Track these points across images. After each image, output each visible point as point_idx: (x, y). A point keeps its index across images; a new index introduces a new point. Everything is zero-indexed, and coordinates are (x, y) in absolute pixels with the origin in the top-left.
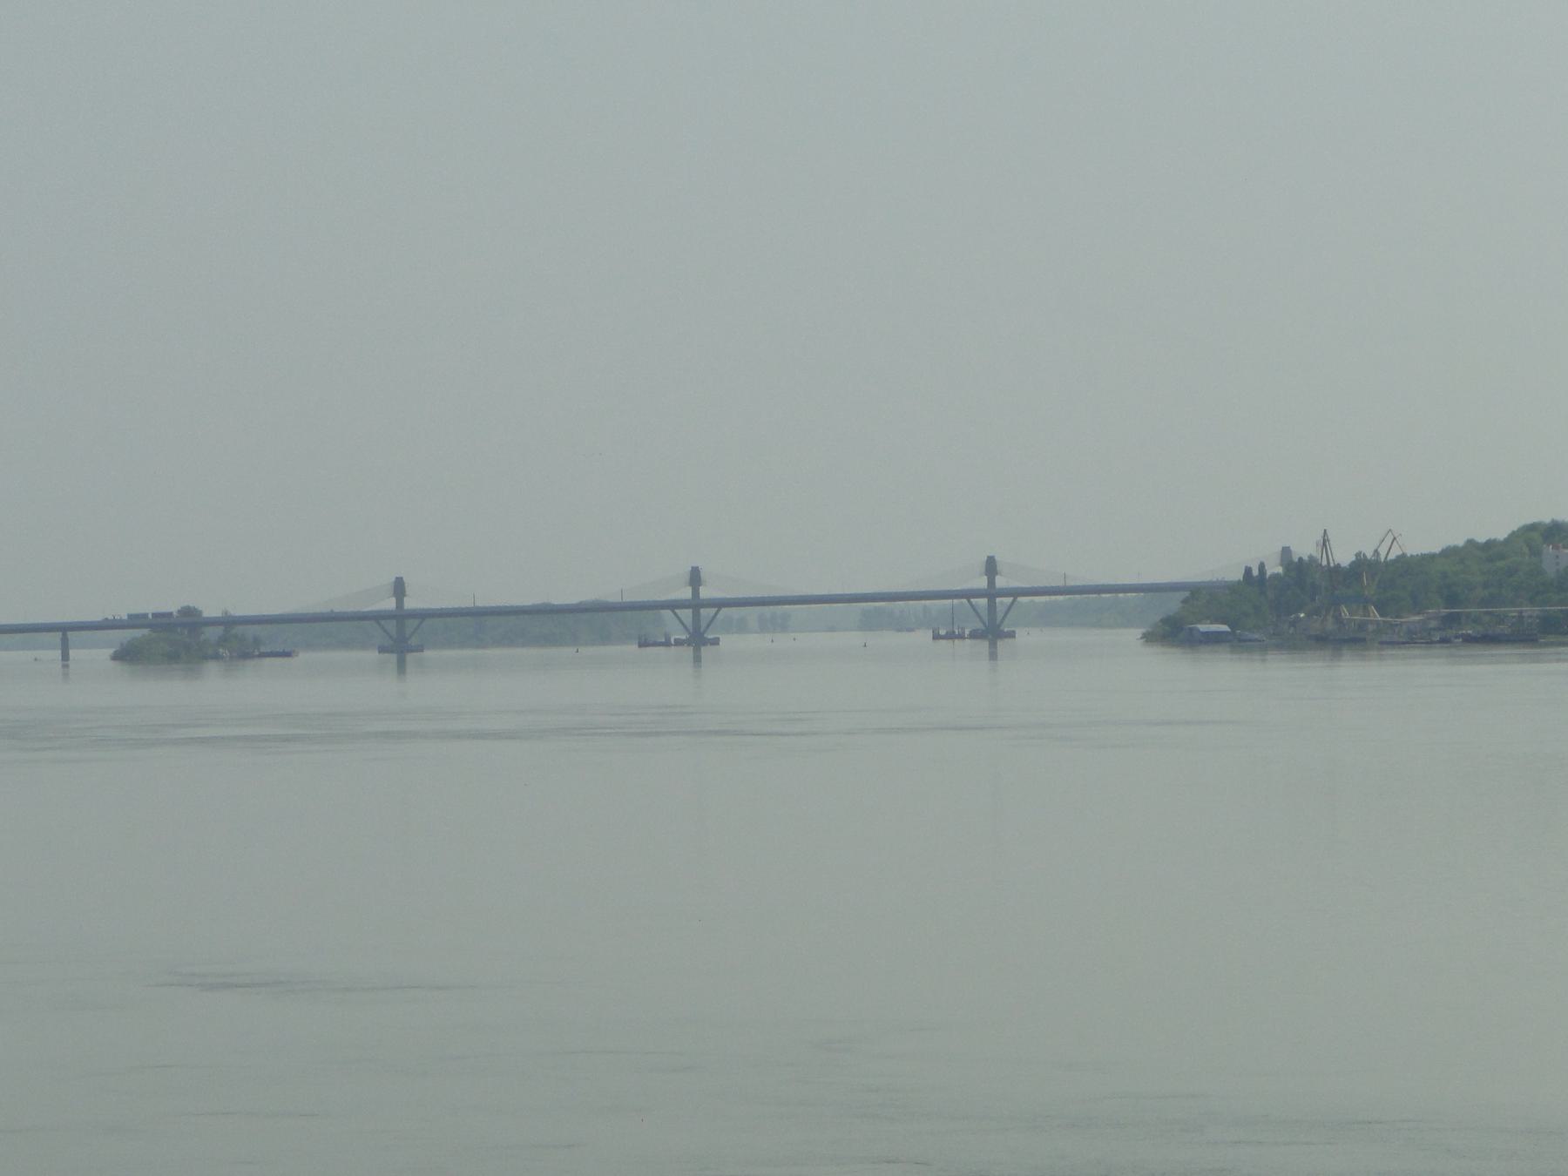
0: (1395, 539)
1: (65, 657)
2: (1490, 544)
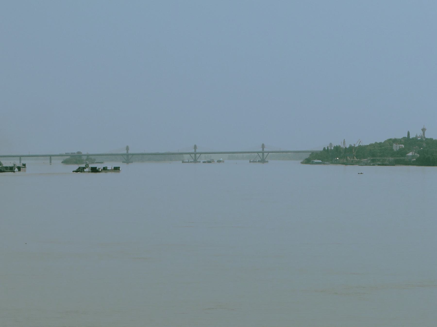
0: (360, 141)
1: (51, 162)
2: (380, 143)
